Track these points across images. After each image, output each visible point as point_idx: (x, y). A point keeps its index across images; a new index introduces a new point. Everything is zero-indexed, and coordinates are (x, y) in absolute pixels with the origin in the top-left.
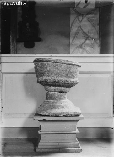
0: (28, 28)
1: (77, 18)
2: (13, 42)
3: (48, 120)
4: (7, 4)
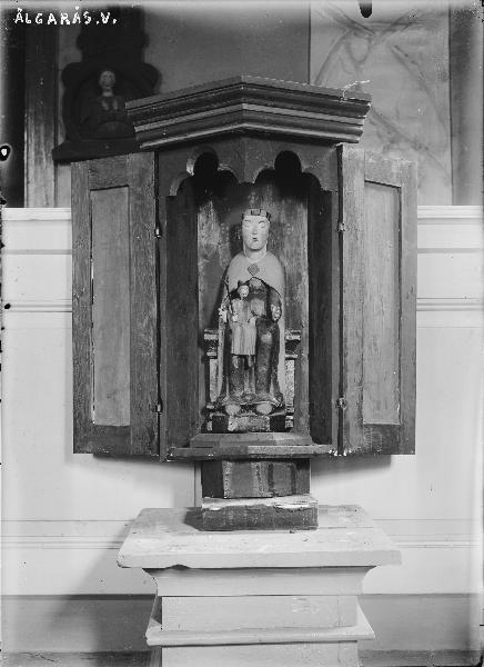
0: (107, 94)
1: (342, 47)
2: (38, 161)
3: (127, 595)
4: (24, 19)
